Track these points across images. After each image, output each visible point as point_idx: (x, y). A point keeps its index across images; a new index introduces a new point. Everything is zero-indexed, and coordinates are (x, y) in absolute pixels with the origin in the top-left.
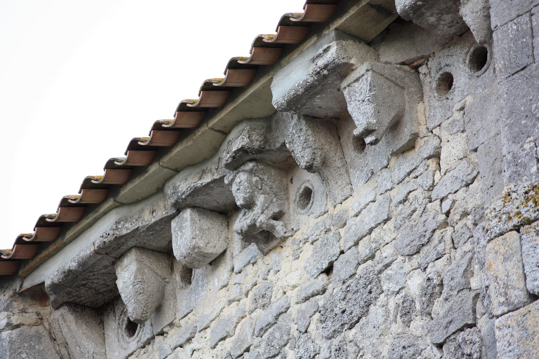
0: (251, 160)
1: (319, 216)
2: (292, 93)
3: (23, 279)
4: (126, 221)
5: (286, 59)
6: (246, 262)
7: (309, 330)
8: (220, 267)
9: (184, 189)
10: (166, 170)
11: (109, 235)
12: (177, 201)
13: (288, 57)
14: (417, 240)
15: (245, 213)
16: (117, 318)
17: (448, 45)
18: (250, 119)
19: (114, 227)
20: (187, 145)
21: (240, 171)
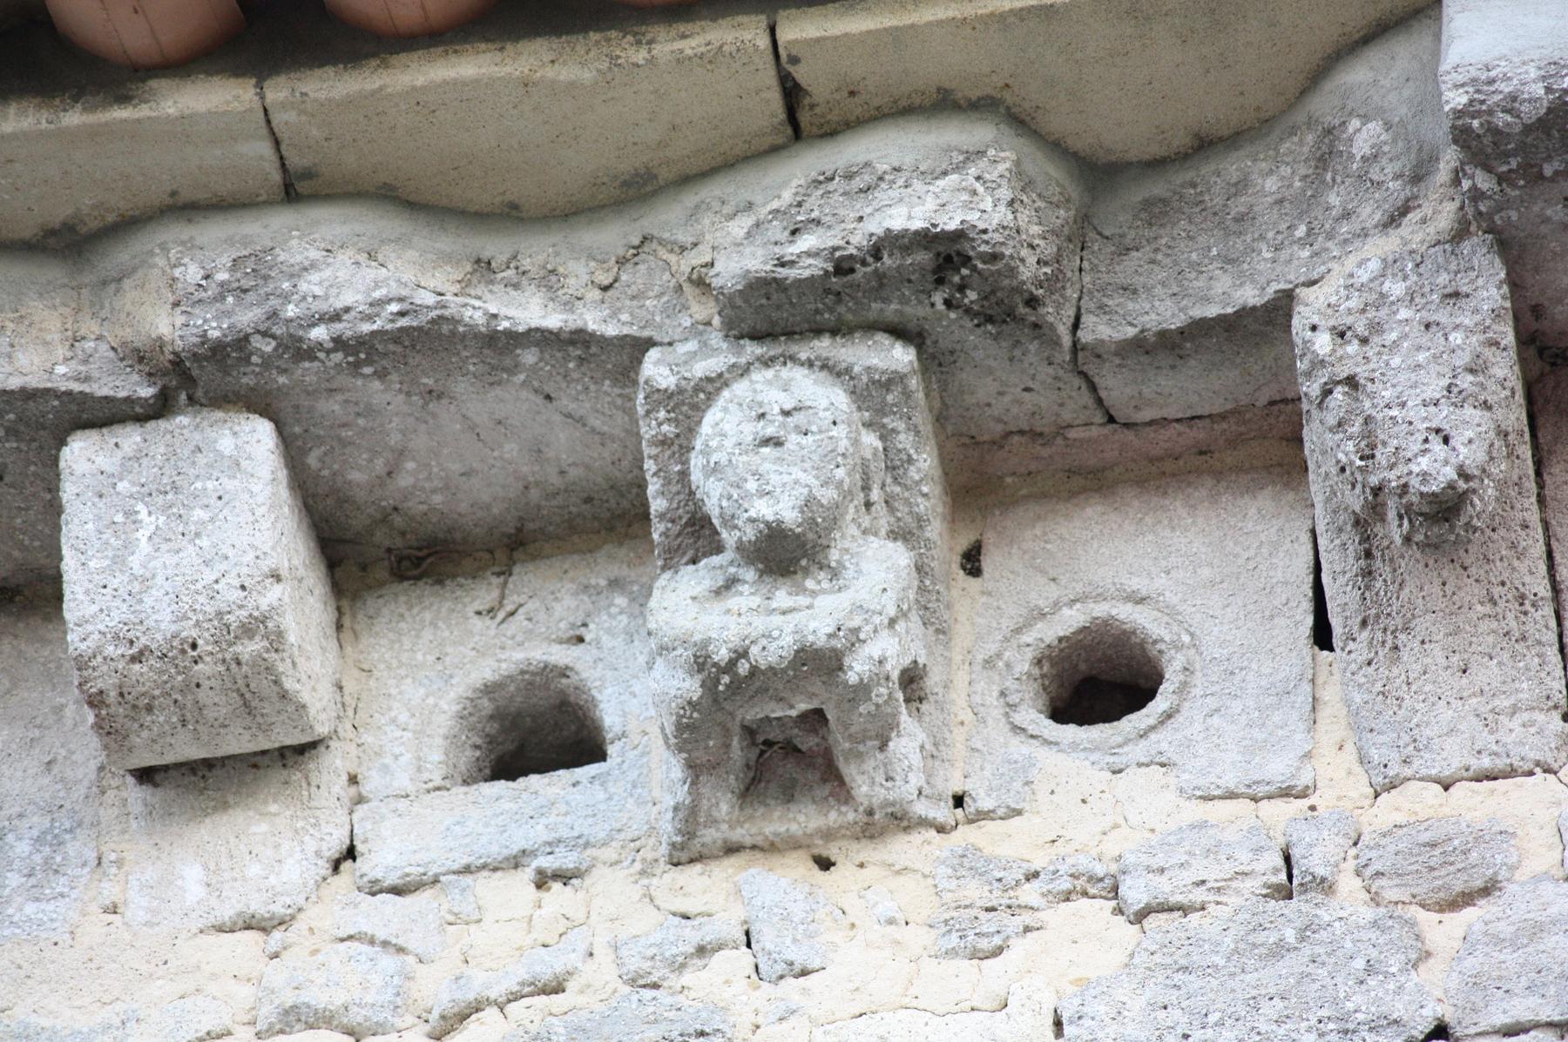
0: (899, 332)
1: (1231, 795)
6: (496, 850)
9: (348, 298)
10: (265, 148)
12: (242, 341)
15: (731, 583)
18: (1020, 122)
20: (550, 73)
21: (793, 358)
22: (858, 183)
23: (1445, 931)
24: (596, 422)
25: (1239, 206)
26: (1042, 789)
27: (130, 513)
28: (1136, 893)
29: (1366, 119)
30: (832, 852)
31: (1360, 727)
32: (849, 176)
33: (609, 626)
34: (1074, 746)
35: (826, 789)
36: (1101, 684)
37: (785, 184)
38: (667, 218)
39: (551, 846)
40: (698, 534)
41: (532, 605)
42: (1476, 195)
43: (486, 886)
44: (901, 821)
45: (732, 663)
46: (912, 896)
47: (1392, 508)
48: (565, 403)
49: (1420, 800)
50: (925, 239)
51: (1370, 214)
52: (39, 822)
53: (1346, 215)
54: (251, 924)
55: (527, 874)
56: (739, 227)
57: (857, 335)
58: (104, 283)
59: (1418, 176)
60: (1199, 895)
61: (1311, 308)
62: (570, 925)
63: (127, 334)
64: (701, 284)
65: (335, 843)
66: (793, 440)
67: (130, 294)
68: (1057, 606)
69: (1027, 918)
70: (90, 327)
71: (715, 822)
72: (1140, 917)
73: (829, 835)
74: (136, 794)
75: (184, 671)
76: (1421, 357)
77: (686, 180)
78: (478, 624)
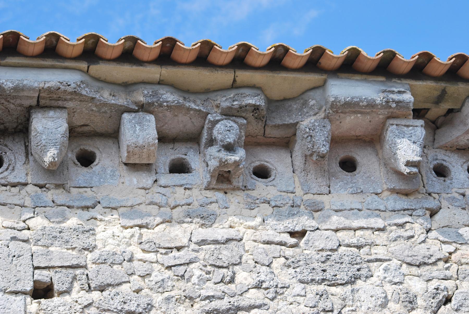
0: (244, 118)
1: (284, 192)
2: (355, 100)
4: (87, 86)
5: (346, 75)
8: (136, 174)
9: (169, 99)
10: (159, 76)
11: (69, 85)
13: (350, 75)
14: (421, 257)
17: (445, 148)
19: (79, 84)
21: (230, 119)
22: (243, 96)
24: (195, 124)
25: (290, 109)
26: (257, 187)
28: (273, 204)
29: (313, 100)
30: (227, 191)
31: (302, 184)
32: (242, 94)
34: (261, 181)
35: (228, 182)
36: (262, 173)
37: (231, 94)
38: (212, 96)
39: (187, 184)
41: (179, 149)
43: (177, 189)
45: (225, 162)
46: (239, 199)
48: (193, 120)
49: (310, 196)
50: (254, 105)
51: (312, 113)
52: (111, 169)
53: (307, 113)
55: (183, 188)
57: (365, 103)
58: (130, 91)
59: (320, 109)
60: (282, 205)
63: (134, 99)
64: (218, 107)
66: (232, 131)
67: (135, 94)
68: (255, 161)
69: (257, 205)
70: (128, 97)
71: (212, 185)
72: (273, 207)
74: (125, 167)
75: (142, 150)
76: (321, 134)
78: (171, 150)
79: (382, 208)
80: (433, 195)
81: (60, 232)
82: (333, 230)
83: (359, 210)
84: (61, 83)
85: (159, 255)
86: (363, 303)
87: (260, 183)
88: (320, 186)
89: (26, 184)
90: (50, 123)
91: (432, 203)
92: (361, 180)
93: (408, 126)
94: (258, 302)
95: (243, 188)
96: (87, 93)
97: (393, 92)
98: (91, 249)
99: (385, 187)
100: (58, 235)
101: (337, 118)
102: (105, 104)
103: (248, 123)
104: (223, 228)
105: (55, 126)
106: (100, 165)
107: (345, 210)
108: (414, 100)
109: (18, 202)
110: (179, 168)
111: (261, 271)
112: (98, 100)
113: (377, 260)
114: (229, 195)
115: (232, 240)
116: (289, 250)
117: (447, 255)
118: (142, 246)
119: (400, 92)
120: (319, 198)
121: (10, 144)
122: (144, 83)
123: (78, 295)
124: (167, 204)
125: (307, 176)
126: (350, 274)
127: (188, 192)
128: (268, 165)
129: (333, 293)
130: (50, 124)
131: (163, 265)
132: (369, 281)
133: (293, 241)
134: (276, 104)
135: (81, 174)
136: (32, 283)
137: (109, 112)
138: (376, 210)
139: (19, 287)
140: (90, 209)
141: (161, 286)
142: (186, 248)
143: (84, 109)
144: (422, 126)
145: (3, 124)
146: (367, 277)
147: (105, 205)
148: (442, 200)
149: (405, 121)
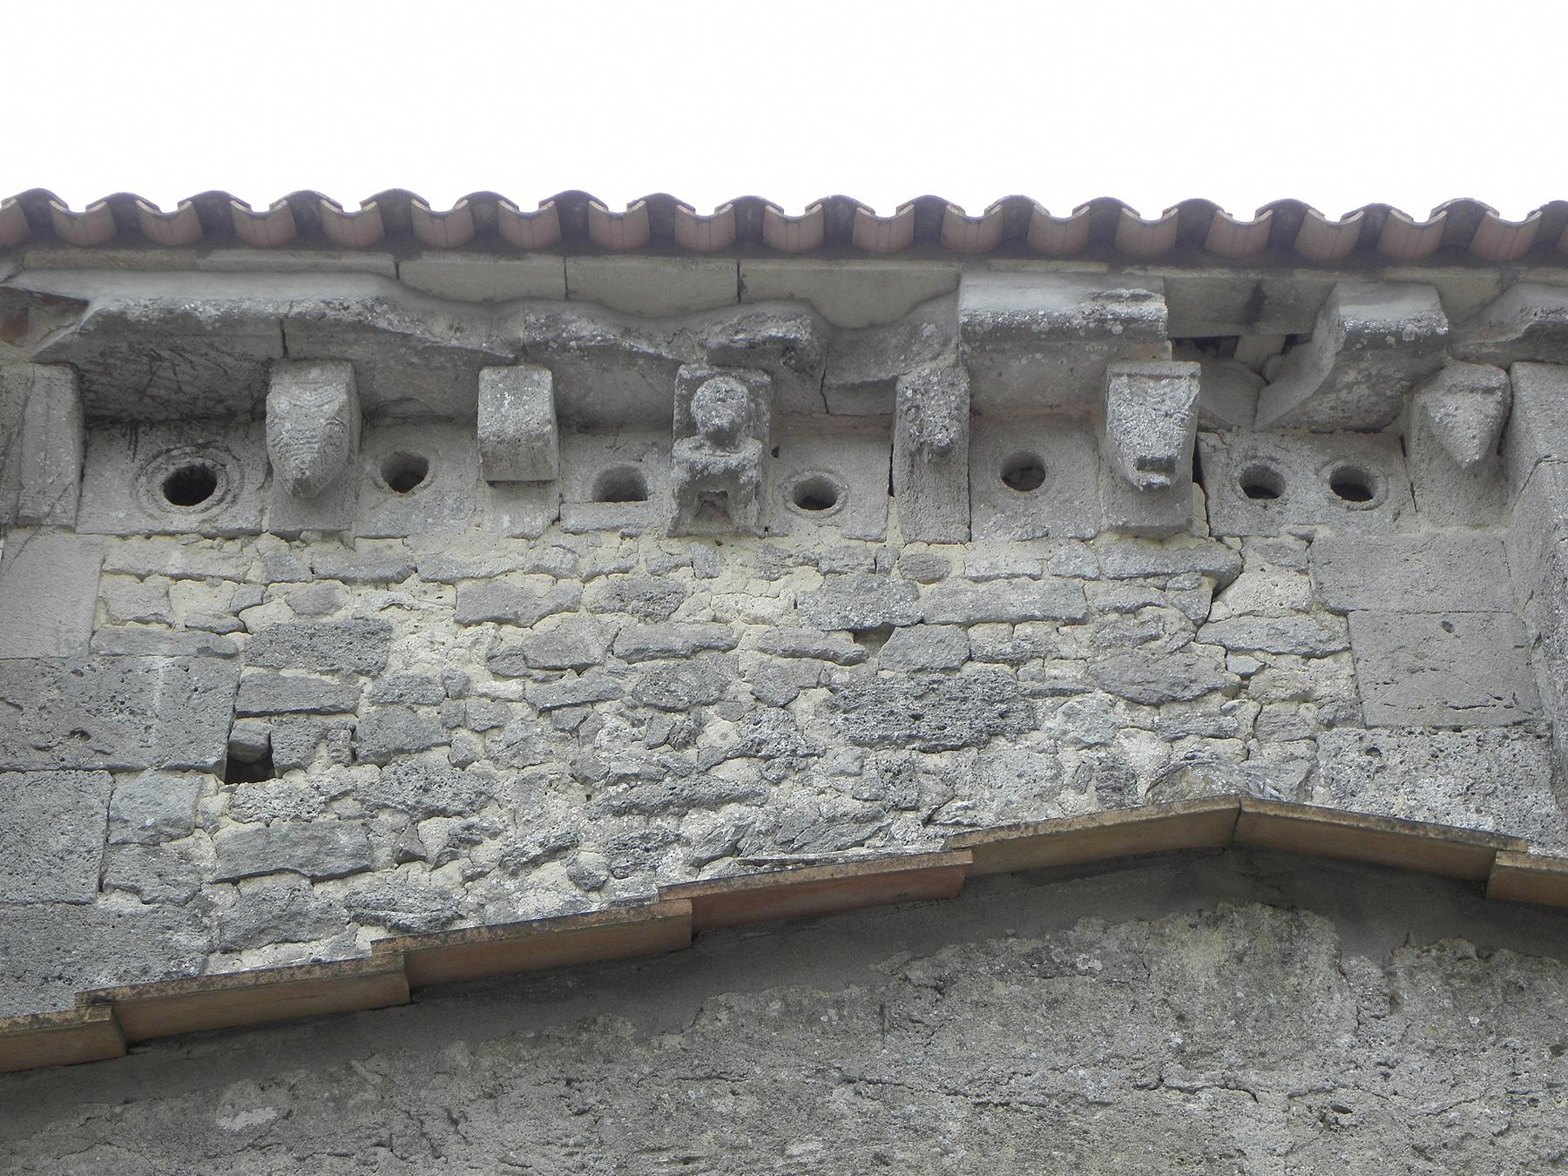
0: (766, 372)
3: (22, 269)
4: (393, 309)
7: (793, 706)
9: (585, 333)
10: (562, 281)
11: (346, 309)
12: (547, 343)
13: (1021, 261)
14: (1165, 685)
15: (700, 446)
16: (140, 456)
17: (1281, 431)
23: (925, 590)
27: (502, 395)
28: (825, 566)
31: (903, 520)
33: (651, 459)
36: (816, 499)
39: (627, 526)
40: (690, 428)
42: (964, 353)
43: (604, 536)
44: (746, 533)
46: (747, 556)
47: (926, 449)
49: (919, 548)
50: (783, 340)
54: (524, 536)
56: (718, 329)
57: (1044, 325)
59: (945, 344)
61: (905, 380)
62: (631, 552)
64: (702, 346)
65: (554, 514)
70: (495, 332)
73: (722, 534)
74: (488, 490)
77: (699, 312)
79: (1090, 571)
80: (1228, 540)
81: (312, 636)
82: (959, 624)
83: (1034, 578)
84: (328, 304)
85: (529, 684)
86: (996, 792)
87: (805, 520)
88: (945, 525)
89: (256, 534)
90: (307, 395)
91: (1220, 559)
92: (1047, 509)
93: (1158, 378)
94: (743, 788)
95: (761, 532)
96: (390, 324)
97: (1118, 299)
98: (375, 673)
99: (1105, 522)
100: (305, 642)
101: (987, 363)
102: (437, 350)
103: (774, 382)
104: (695, 622)
105: (319, 401)
106: (433, 488)
107: (998, 577)
108: (1169, 313)
109: (232, 572)
110: (622, 490)
111: (764, 718)
112: (419, 340)
113: (1055, 692)
114: (725, 549)
115: (709, 648)
116: (843, 671)
117: (1238, 679)
118: (495, 666)
119: (1136, 298)
120: (937, 551)
121: (236, 448)
122: (531, 298)
123: (325, 773)
124: (573, 570)
125: (916, 501)
126: (979, 724)
127: (628, 543)
128: (832, 478)
129: (931, 767)
130: (308, 397)
131: (533, 705)
132: (1024, 743)
133: (856, 648)
134: (839, 339)
135: (385, 509)
136: (222, 749)
137: (449, 365)
138: (1076, 576)
139: (192, 757)
140: (393, 585)
141: (519, 750)
142: (596, 669)
143: (392, 362)
144: (1193, 376)
145: (221, 401)
146: (1020, 732)
147: (425, 575)
148: (1250, 553)
149: (1152, 365)
